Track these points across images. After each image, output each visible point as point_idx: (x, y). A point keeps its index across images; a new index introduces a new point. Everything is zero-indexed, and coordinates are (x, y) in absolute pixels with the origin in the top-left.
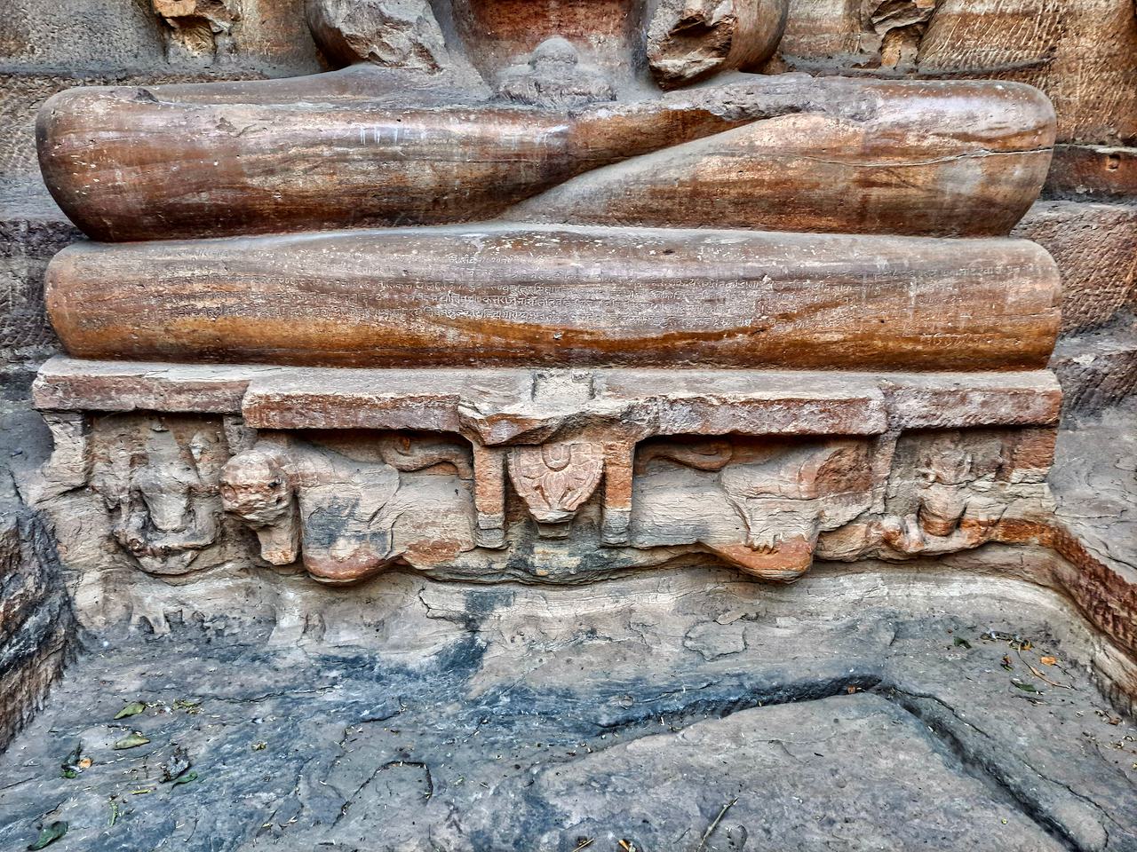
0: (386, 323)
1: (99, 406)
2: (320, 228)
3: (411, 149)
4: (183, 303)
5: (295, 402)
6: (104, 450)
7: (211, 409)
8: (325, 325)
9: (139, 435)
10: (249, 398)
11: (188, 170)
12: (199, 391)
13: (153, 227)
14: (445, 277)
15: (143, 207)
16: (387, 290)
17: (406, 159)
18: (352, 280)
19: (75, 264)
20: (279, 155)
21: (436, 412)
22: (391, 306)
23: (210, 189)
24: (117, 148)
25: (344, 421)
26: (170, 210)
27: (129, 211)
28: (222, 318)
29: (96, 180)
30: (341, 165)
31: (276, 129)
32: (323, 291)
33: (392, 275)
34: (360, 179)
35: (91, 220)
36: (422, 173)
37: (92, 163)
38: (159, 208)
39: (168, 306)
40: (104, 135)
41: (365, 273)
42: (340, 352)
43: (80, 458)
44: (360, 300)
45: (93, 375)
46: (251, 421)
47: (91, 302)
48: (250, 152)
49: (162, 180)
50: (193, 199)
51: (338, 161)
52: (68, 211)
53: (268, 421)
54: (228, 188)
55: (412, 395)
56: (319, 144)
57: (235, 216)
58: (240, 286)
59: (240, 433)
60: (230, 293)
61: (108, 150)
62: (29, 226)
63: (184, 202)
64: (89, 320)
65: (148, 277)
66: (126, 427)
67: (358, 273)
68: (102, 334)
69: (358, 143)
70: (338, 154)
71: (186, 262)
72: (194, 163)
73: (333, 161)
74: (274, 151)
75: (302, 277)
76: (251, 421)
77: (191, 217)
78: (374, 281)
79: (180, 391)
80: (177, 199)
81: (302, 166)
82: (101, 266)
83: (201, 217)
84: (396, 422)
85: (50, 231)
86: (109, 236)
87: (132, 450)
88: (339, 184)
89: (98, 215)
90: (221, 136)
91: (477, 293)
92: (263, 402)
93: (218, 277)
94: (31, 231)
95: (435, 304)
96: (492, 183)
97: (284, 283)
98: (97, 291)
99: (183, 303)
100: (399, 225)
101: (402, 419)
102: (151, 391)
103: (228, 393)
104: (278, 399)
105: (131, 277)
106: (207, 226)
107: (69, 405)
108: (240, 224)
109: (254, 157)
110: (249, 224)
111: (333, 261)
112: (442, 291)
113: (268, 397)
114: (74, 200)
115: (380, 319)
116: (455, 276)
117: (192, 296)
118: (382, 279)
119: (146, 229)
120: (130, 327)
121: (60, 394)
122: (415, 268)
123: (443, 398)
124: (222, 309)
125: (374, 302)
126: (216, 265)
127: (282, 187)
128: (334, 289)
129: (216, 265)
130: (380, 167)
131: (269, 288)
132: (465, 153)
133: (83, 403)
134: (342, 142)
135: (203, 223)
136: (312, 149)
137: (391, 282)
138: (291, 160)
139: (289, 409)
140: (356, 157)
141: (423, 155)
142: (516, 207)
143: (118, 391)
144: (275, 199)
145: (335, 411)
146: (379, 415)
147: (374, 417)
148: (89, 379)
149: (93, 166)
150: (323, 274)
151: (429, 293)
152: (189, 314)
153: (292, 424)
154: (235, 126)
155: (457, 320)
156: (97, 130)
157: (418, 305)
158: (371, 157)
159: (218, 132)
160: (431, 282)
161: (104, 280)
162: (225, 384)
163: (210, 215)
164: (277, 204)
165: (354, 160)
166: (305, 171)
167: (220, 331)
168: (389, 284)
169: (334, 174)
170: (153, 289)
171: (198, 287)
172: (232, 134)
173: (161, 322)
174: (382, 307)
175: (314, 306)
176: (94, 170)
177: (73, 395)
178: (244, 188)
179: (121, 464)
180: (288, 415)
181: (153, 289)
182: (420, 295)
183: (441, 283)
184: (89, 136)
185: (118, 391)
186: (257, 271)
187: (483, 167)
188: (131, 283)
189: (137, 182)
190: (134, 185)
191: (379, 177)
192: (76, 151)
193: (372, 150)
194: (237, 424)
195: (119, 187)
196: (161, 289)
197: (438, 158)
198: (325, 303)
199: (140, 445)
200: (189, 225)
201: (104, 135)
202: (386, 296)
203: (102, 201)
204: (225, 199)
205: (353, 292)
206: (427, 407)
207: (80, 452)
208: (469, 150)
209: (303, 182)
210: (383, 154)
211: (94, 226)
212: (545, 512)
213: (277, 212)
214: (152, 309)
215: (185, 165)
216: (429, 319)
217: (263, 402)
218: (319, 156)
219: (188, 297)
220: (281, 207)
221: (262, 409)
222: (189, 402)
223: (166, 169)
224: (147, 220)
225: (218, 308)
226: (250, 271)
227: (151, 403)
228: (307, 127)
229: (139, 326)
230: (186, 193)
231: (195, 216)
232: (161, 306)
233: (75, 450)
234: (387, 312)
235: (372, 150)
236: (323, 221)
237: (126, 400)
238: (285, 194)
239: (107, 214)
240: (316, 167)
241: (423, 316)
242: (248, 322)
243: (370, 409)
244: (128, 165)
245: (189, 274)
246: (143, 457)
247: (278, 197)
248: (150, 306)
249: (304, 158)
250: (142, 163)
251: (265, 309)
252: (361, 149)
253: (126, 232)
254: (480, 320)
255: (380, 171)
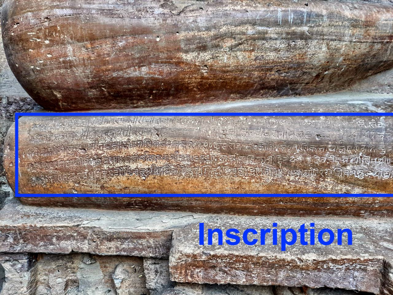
0: (296, 182)
1: (42, 250)
2: (226, 99)
3: (315, 29)
4: (118, 165)
5: (219, 261)
6: (45, 277)
7: (136, 253)
8: (240, 183)
9: (73, 266)
10: (177, 256)
11: (133, 45)
12: (126, 239)
13: (96, 98)
14: (358, 140)
15: (90, 80)
16: (301, 153)
17: (310, 38)
18: (269, 144)
19: (37, 129)
20: (212, 33)
21: (356, 274)
22: (304, 167)
23: (150, 64)
24: (69, 24)
25: (264, 279)
26: (112, 84)
27: (77, 84)
28: (151, 177)
29: (49, 56)
30: (259, 43)
31: (210, 9)
32: (242, 154)
33: (306, 139)
34: (272, 56)
35: (44, 94)
36: (318, 51)
37: (46, 39)
38: (103, 82)
39: (105, 167)
40: (58, 12)
41: (280, 137)
42: (248, 205)
43: (25, 289)
44: (275, 162)
45: (38, 225)
46: (177, 276)
47: (40, 162)
48: (188, 29)
49: (109, 55)
50: (134, 73)
51: (259, 39)
52: (28, 86)
53: (192, 276)
54: (165, 63)
55: (334, 258)
56: (246, 23)
57: (166, 89)
58: (170, 149)
59: (156, 272)
60: (160, 156)
61: (62, 26)
62: (8, 100)
63: (126, 76)
64: (38, 178)
65: (89, 142)
66: (63, 260)
67: (274, 137)
68: (48, 189)
69: (276, 24)
70: (259, 33)
71: (123, 129)
72: (139, 38)
73: (254, 39)
74: (208, 29)
75: (223, 141)
76: (177, 276)
77: (130, 90)
78: (289, 144)
79: (110, 239)
80: (120, 73)
81: (229, 43)
82: (50, 132)
83: (138, 90)
84: (315, 282)
85: (21, 103)
86: (58, 106)
87: (67, 276)
88: (255, 60)
89: (49, 88)
90: (164, 14)
91: (387, 156)
92: (190, 260)
93: (150, 141)
94: (9, 103)
95: (345, 165)
96: (363, 61)
97: (208, 148)
98: (46, 152)
99: (118, 165)
100: (287, 95)
101: (322, 279)
102: (85, 238)
103: (151, 241)
104: (204, 258)
105: (75, 142)
106: (141, 97)
107: (18, 249)
108: (168, 95)
109: (191, 33)
110: (175, 96)
111: (251, 127)
112: (354, 153)
113: (195, 256)
114: (29, 75)
115: (292, 178)
116: (367, 140)
117: (127, 158)
118: (297, 143)
119: (89, 100)
120: (72, 184)
121: (10, 240)
122: (327, 133)
123: (366, 261)
124: (152, 170)
125: (287, 164)
126: (149, 131)
127: (210, 62)
128: (252, 152)
129: (149, 131)
130: (289, 45)
131: (195, 151)
132: (353, 35)
133: (29, 247)
134: (265, 22)
135: (138, 95)
136: (239, 28)
137: (304, 146)
138: (221, 37)
139: (214, 267)
140: (272, 36)
141: (323, 35)
142: (365, 81)
143: (59, 238)
144: (203, 74)
145: (256, 271)
146: (299, 275)
147: (294, 277)
148: (35, 228)
149: (47, 42)
150: (242, 138)
151: (340, 156)
152: (123, 173)
153: (214, 280)
154: (176, 5)
155: (365, 180)
156: (52, 7)
157: (329, 166)
158: (284, 36)
159: (161, 10)
160: (343, 145)
161: (52, 144)
162: (149, 234)
163: (145, 88)
164: (203, 78)
165: (271, 38)
166: (231, 48)
167: (148, 188)
168: (304, 147)
169: (253, 50)
170: (93, 152)
171: (133, 151)
172: (174, 12)
173: (98, 180)
174: (295, 167)
175: (233, 167)
176: (47, 46)
177: (21, 241)
178: (179, 63)
179: (58, 289)
180: (212, 272)
181: (93, 152)
182: (332, 158)
183: (353, 147)
184: (44, 14)
185: (59, 238)
186: (185, 137)
187: (363, 46)
188: (75, 147)
189: (86, 57)
190: (84, 60)
191: (287, 54)
192: (31, 28)
193: (286, 29)
194: (155, 263)
195: (70, 62)
196: (100, 152)
197: (334, 37)
198: (243, 165)
199: (73, 273)
200: (126, 96)
201: (58, 12)
202: (300, 158)
203: (54, 75)
204: (161, 73)
205: (269, 155)
206: (347, 269)
207: (25, 285)
208: (357, 31)
209: (227, 58)
210: (294, 33)
211: (47, 100)
212: (250, 233)
213: (201, 85)
214: (91, 170)
215: (131, 40)
216: (337, 179)
217: (190, 260)
218: (244, 34)
219: (124, 159)
220: (204, 81)
221: (187, 266)
222: (117, 248)
223: (114, 45)
224: (92, 93)
225: (149, 169)
226: (178, 136)
227: (85, 247)
228: (236, 8)
229: (79, 183)
230: (129, 67)
231: (134, 89)
232: (100, 167)
233: (21, 283)
234: (299, 172)
235: (286, 29)
236: (231, 93)
237: (65, 245)
238: (211, 69)
239: (58, 88)
240: (240, 44)
241: (333, 176)
242: (173, 181)
243: (291, 270)
244: (78, 41)
245: (125, 139)
246: (75, 282)
247: (204, 71)
248: (90, 167)
249: (232, 36)
250: (92, 38)
251: (190, 169)
252: (279, 29)
253: (73, 103)
254: (386, 180)
255: (289, 48)
